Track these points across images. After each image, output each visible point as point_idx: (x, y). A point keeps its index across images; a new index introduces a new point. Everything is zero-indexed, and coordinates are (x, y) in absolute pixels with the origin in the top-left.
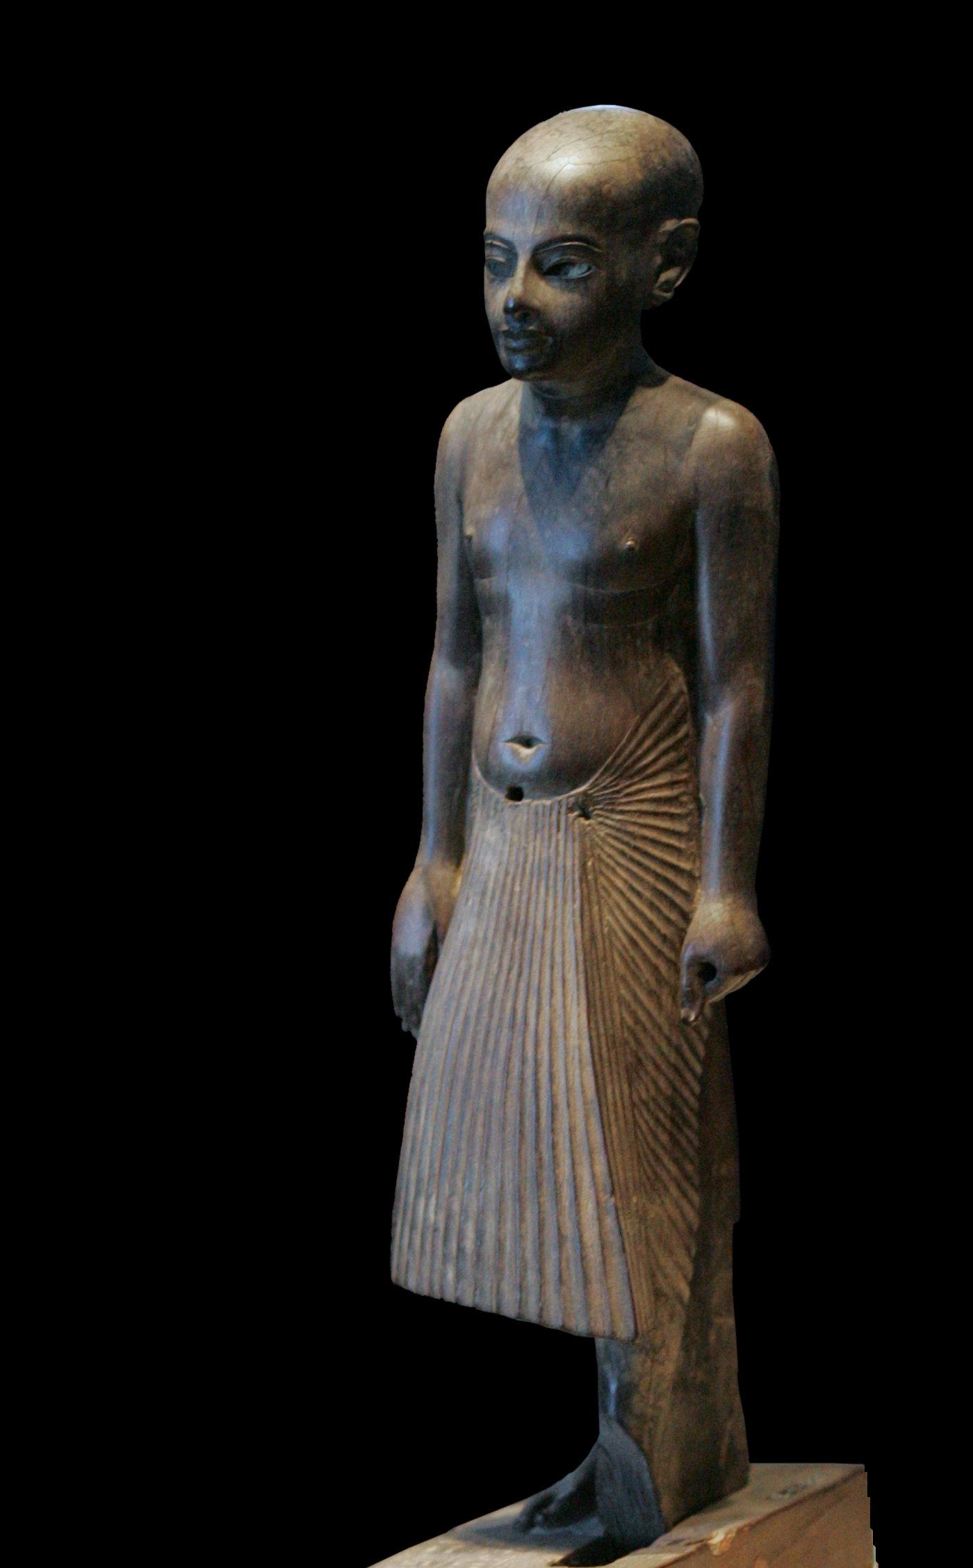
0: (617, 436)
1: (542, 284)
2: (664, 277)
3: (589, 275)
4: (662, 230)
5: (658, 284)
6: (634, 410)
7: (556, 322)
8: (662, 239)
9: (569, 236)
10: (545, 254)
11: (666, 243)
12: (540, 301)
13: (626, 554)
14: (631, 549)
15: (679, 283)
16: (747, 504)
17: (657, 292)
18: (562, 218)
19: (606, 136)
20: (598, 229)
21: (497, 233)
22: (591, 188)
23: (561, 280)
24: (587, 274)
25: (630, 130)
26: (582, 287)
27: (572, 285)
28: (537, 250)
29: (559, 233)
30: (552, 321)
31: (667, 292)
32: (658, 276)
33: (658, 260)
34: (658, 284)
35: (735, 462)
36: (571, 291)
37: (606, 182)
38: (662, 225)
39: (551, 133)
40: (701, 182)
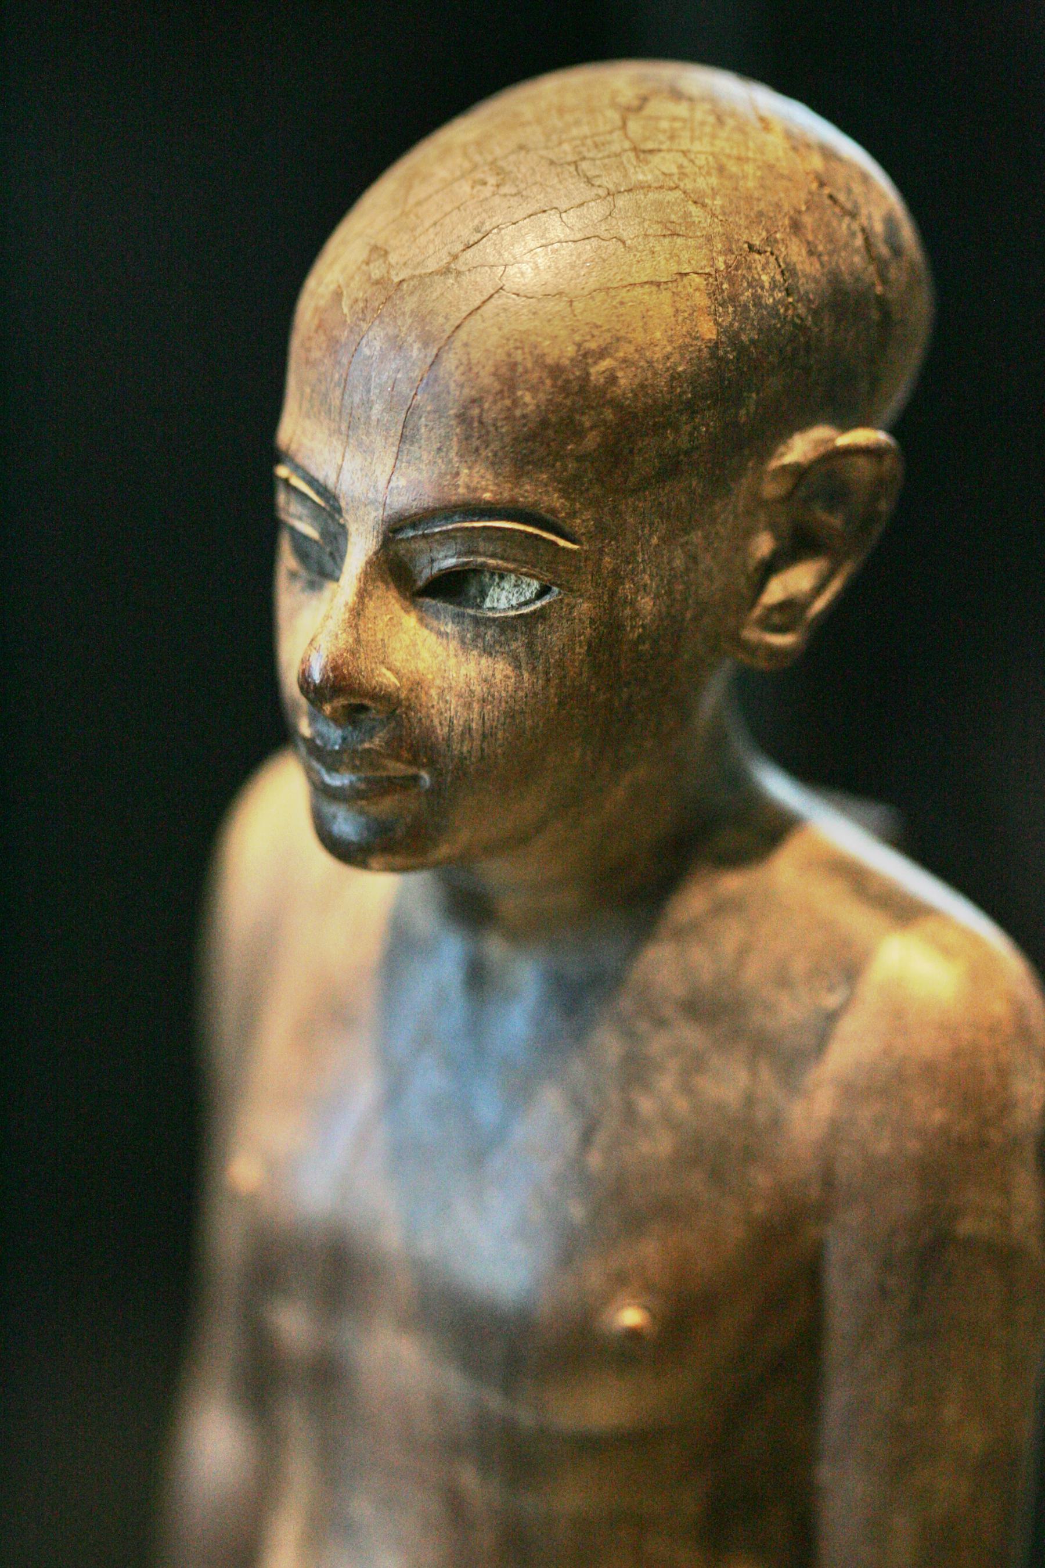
0: (626, 1003)
1: (410, 621)
2: (776, 591)
3: (543, 608)
4: (774, 464)
5: (757, 612)
6: (680, 934)
7: (441, 732)
8: (771, 490)
9: (488, 502)
10: (422, 544)
11: (790, 496)
12: (397, 673)
13: (884, 299)
14: (633, 1334)
15: (820, 604)
16: (966, 1227)
17: (752, 634)
18: (470, 452)
19: (621, 201)
20: (569, 487)
21: (301, 459)
22: (556, 371)
23: (458, 618)
24: (538, 604)
25: (701, 183)
26: (517, 645)
27: (490, 634)
28: (396, 531)
29: (460, 493)
30: (431, 730)
31: (779, 629)
32: (760, 586)
33: (764, 545)
34: (757, 612)
35: (938, 1116)
36: (488, 651)
37: (602, 353)
38: (782, 449)
39: (479, 175)
40: (908, 233)
